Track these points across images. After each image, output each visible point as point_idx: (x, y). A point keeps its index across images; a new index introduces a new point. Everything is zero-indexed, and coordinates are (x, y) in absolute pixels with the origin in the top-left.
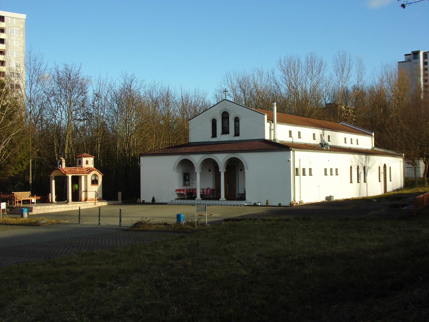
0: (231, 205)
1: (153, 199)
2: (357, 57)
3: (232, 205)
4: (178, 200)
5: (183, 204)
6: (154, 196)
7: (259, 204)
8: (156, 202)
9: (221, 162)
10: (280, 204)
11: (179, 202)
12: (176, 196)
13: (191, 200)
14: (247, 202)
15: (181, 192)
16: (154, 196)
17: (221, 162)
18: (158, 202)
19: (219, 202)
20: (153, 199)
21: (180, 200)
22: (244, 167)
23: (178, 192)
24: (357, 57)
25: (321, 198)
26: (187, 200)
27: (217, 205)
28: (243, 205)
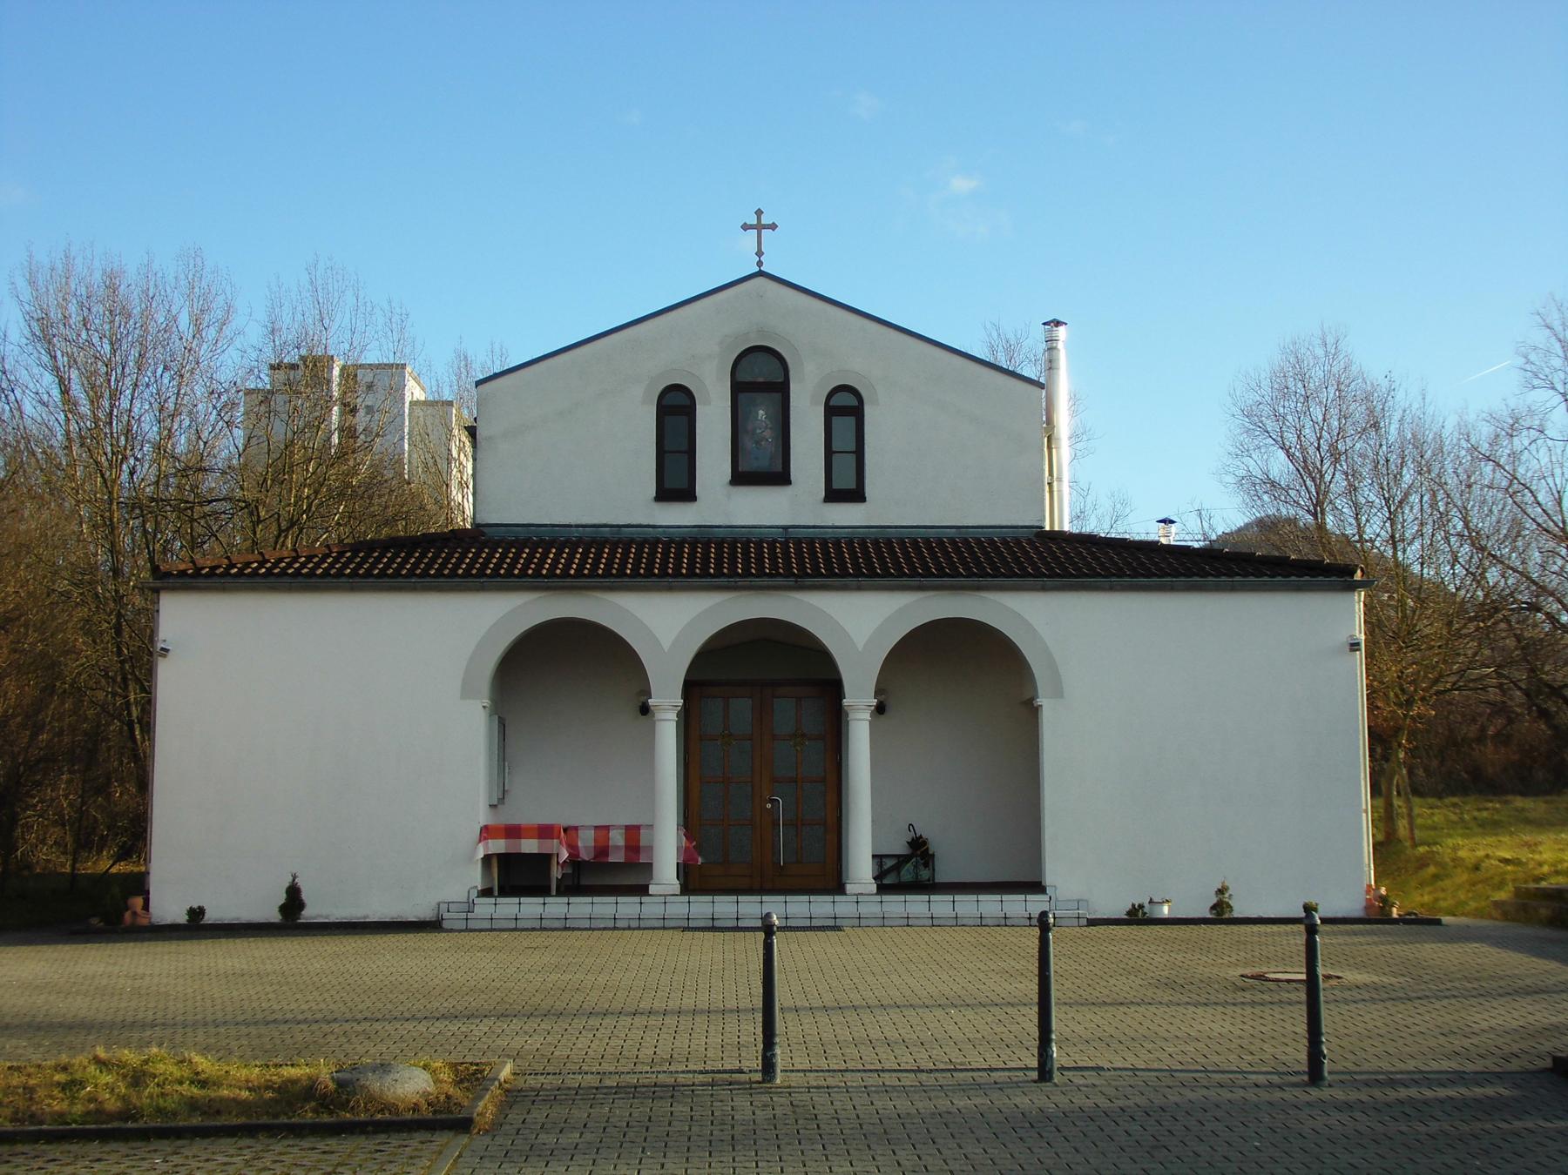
0: (981, 922)
1: (293, 900)
2: (390, 302)
3: (989, 922)
4: (548, 900)
5: (586, 924)
6: (294, 877)
7: (1165, 911)
8: (311, 913)
9: (666, 643)
10: (196, 913)
11: (886, 908)
12: (475, 877)
13: (588, 896)
14: (1056, 900)
15: (523, 841)
16: (294, 877)
17: (666, 643)
18: (321, 916)
19: (842, 906)
20: (293, 900)
21: (565, 900)
22: (1029, 665)
23: (498, 846)
24: (390, 302)
25: (285, 895)
26: (500, 900)
27: (872, 923)
28: (1075, 922)
